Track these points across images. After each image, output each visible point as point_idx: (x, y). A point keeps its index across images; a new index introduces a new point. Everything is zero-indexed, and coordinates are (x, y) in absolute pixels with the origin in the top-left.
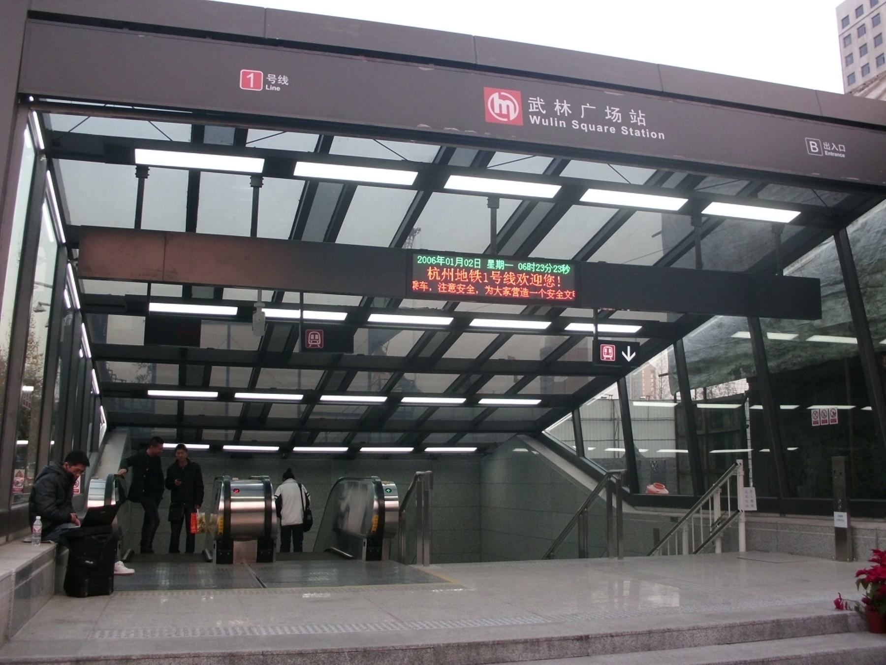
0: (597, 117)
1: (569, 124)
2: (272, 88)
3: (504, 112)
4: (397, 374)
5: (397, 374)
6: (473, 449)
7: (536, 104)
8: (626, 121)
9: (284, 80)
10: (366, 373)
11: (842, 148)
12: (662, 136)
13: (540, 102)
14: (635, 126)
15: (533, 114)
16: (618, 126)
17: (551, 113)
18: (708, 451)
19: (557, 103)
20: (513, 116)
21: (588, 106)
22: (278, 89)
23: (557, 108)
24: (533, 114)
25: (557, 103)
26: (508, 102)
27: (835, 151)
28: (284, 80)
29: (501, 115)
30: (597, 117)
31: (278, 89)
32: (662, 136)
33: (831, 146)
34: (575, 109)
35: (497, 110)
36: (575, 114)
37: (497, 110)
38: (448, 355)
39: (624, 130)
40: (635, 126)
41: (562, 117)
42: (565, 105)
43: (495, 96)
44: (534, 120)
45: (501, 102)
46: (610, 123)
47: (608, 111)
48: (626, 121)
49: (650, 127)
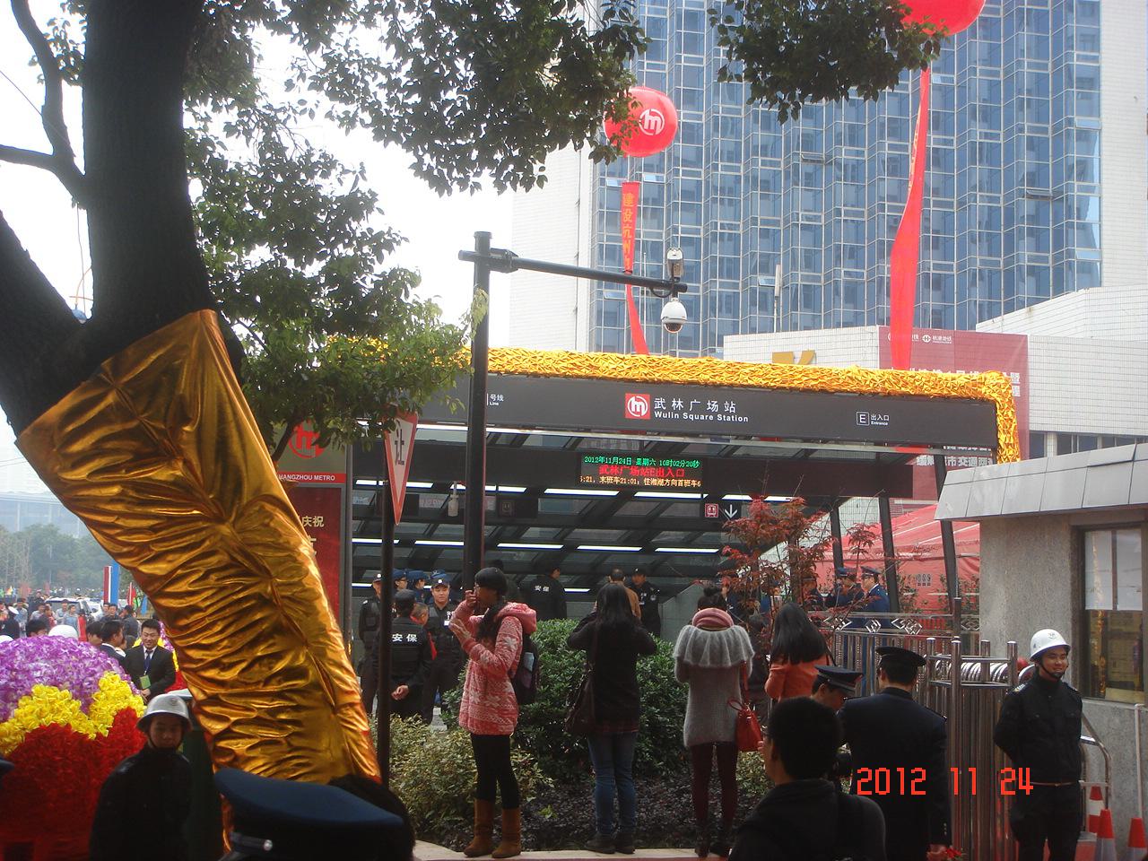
0: (700, 409)
1: (681, 416)
2: (494, 404)
3: (638, 410)
4: (432, 525)
5: (432, 525)
6: (549, 491)
7: (660, 402)
8: (721, 410)
9: (501, 398)
10: (1107, 535)
11: (887, 417)
12: (746, 419)
13: (662, 401)
14: (728, 414)
15: (657, 410)
16: (715, 414)
17: (669, 408)
18: (355, 481)
19: (674, 401)
20: (644, 413)
21: (695, 401)
22: (497, 404)
23: (674, 404)
24: (657, 410)
25: (674, 401)
26: (641, 403)
27: (880, 421)
28: (501, 398)
29: (649, 130)
30: (700, 409)
31: (497, 404)
32: (746, 419)
33: (878, 417)
34: (686, 405)
35: (633, 409)
36: (686, 409)
37: (633, 409)
38: (620, 513)
39: (720, 417)
40: (728, 414)
41: (676, 411)
42: (679, 402)
43: (633, 399)
44: (658, 414)
45: (636, 403)
46: (710, 413)
47: (709, 404)
48: (721, 410)
49: (738, 413)
